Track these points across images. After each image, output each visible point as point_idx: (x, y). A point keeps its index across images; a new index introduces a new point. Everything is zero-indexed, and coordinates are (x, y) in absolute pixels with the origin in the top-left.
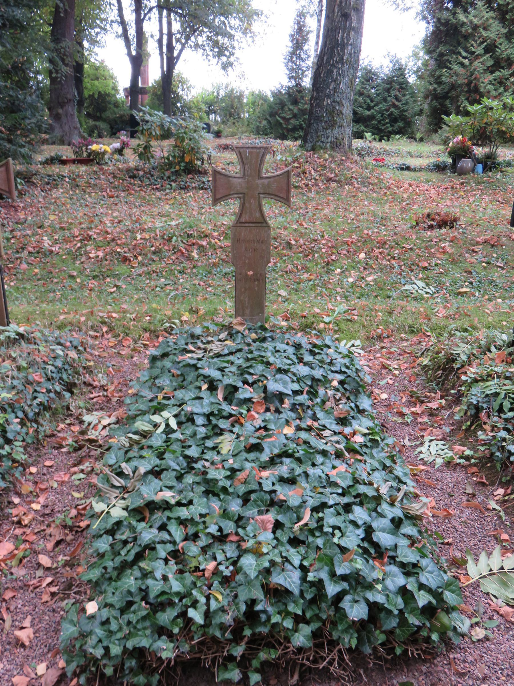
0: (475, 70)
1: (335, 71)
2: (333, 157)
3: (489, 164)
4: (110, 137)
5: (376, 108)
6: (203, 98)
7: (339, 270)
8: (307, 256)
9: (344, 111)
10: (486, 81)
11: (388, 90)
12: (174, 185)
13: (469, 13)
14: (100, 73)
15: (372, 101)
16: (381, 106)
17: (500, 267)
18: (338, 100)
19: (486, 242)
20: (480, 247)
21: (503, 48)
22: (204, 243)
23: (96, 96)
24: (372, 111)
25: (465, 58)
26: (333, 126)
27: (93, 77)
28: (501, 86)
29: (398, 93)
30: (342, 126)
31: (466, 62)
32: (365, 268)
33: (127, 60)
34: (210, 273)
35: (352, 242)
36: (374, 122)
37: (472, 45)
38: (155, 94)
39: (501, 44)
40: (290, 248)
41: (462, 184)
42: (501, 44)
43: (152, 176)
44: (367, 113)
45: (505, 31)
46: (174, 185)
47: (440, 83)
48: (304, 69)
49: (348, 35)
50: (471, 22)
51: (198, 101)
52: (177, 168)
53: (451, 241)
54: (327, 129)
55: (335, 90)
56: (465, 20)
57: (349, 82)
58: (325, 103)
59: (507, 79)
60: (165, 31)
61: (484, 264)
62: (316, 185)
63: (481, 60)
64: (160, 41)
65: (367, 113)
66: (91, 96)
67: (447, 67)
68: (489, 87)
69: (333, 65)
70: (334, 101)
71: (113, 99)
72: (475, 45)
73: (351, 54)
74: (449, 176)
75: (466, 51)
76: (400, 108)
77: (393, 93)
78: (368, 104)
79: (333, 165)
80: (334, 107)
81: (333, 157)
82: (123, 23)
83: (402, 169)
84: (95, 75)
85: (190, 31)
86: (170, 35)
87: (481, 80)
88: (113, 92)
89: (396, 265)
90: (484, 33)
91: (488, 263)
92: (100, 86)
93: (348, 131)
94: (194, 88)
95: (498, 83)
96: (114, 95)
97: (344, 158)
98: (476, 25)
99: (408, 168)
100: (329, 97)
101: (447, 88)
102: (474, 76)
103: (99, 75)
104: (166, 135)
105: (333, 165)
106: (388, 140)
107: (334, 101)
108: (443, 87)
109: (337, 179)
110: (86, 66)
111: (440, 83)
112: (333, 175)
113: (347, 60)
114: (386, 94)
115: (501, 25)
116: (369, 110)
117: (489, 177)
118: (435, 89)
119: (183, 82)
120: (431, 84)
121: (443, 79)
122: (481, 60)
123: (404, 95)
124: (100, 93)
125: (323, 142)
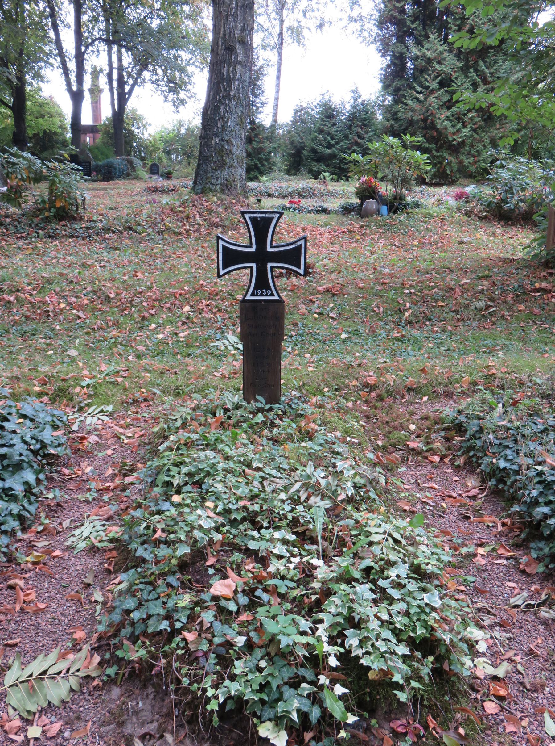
0: (430, 105)
1: (222, 107)
2: (222, 200)
3: (396, 205)
4: (288, 172)
5: (338, 146)
6: (162, 137)
7: (154, 326)
8: (123, 310)
9: (234, 150)
10: (443, 117)
11: (350, 127)
12: (41, 232)
13: (423, 46)
14: (46, 109)
15: (332, 139)
16: (342, 143)
17: (332, 318)
18: (227, 138)
19: (328, 290)
20: (319, 296)
21: (459, 82)
22: (12, 299)
23: (41, 135)
24: (333, 149)
25: (420, 93)
26: (222, 166)
27: (37, 115)
28: (459, 122)
29: (360, 130)
30: (232, 166)
31: (421, 97)
32: (184, 323)
33: (67, 96)
34: (7, 332)
35: (180, 295)
36: (336, 161)
37: (426, 80)
38: (107, 133)
39: (456, 78)
40: (109, 302)
41: (362, 227)
42: (456, 78)
43: (20, 223)
44: (328, 151)
45: (460, 64)
46: (41, 232)
47: (397, 120)
48: (258, 105)
49: (234, 69)
50: (424, 56)
51: (154, 140)
52: (47, 214)
53: (291, 291)
54: (216, 170)
55: (223, 128)
56: (418, 53)
57: (239, 119)
58: (213, 142)
59: (465, 115)
60: (115, 65)
61: (316, 315)
62: (198, 230)
63: (436, 95)
64: (110, 76)
65: (328, 151)
66: (35, 135)
67: (402, 103)
68: (446, 123)
69: (220, 101)
70: (222, 140)
71: (60, 138)
72: (429, 79)
73: (238, 89)
74: (351, 219)
75: (421, 86)
76: (362, 146)
77: (354, 130)
78: (329, 142)
79: (220, 209)
80: (223, 146)
81: (222, 200)
82: (61, 54)
83: (318, 212)
84: (39, 112)
85: (142, 64)
86: (121, 69)
87: (437, 116)
88: (59, 131)
89: (219, 319)
90: (437, 67)
91: (321, 314)
92: (44, 123)
93: (241, 172)
94: (150, 125)
95: (456, 119)
96: (62, 134)
97: (234, 201)
98: (429, 59)
99: (325, 211)
100: (216, 135)
101: (405, 124)
102: (430, 112)
103: (42, 112)
104: (38, 178)
105: (220, 209)
106: (347, 180)
107: (222, 140)
108: (400, 123)
109: (222, 223)
110: (29, 103)
111: (397, 120)
112: (218, 220)
113: (234, 96)
114: (348, 131)
115: (456, 58)
116: (330, 148)
117: (392, 219)
118: (392, 126)
119: (137, 119)
120: (388, 120)
121: (400, 115)
122: (436, 95)
123: (367, 133)
124: (45, 132)
125: (212, 184)
